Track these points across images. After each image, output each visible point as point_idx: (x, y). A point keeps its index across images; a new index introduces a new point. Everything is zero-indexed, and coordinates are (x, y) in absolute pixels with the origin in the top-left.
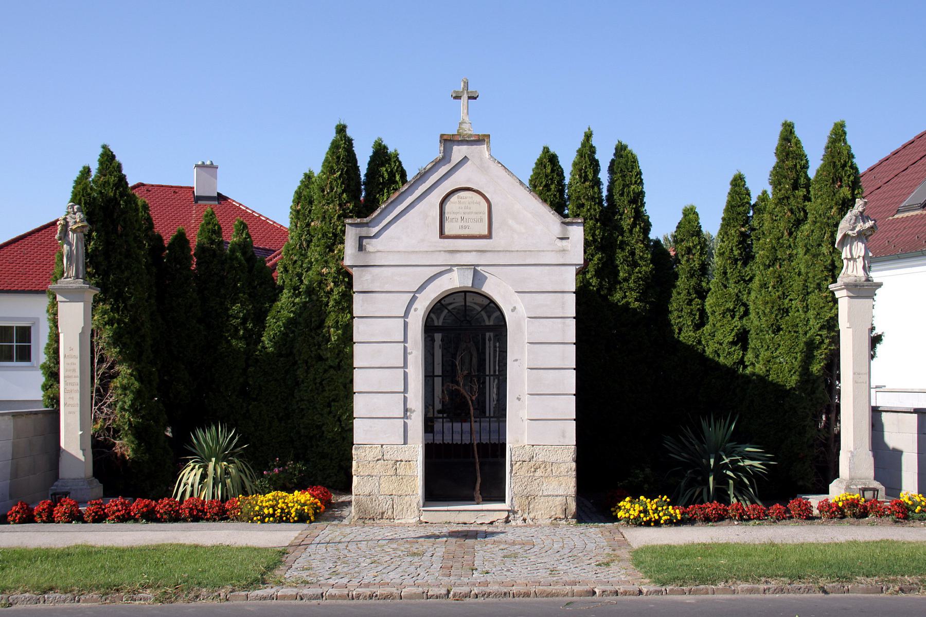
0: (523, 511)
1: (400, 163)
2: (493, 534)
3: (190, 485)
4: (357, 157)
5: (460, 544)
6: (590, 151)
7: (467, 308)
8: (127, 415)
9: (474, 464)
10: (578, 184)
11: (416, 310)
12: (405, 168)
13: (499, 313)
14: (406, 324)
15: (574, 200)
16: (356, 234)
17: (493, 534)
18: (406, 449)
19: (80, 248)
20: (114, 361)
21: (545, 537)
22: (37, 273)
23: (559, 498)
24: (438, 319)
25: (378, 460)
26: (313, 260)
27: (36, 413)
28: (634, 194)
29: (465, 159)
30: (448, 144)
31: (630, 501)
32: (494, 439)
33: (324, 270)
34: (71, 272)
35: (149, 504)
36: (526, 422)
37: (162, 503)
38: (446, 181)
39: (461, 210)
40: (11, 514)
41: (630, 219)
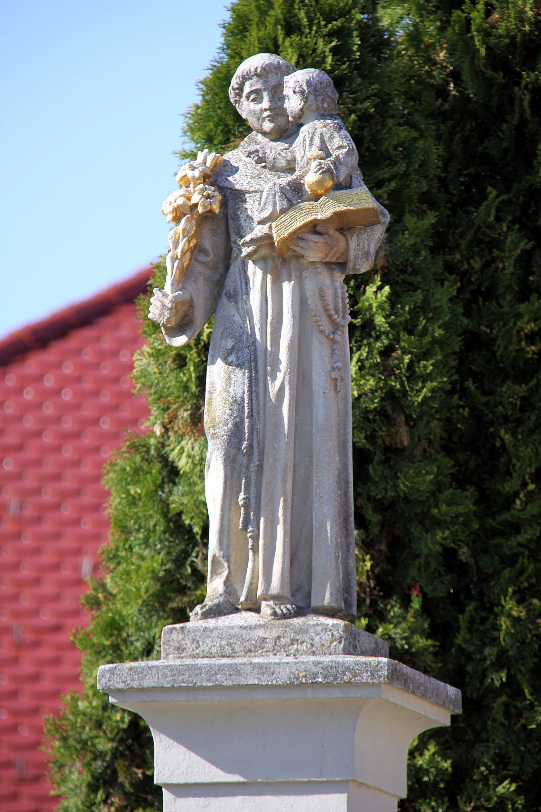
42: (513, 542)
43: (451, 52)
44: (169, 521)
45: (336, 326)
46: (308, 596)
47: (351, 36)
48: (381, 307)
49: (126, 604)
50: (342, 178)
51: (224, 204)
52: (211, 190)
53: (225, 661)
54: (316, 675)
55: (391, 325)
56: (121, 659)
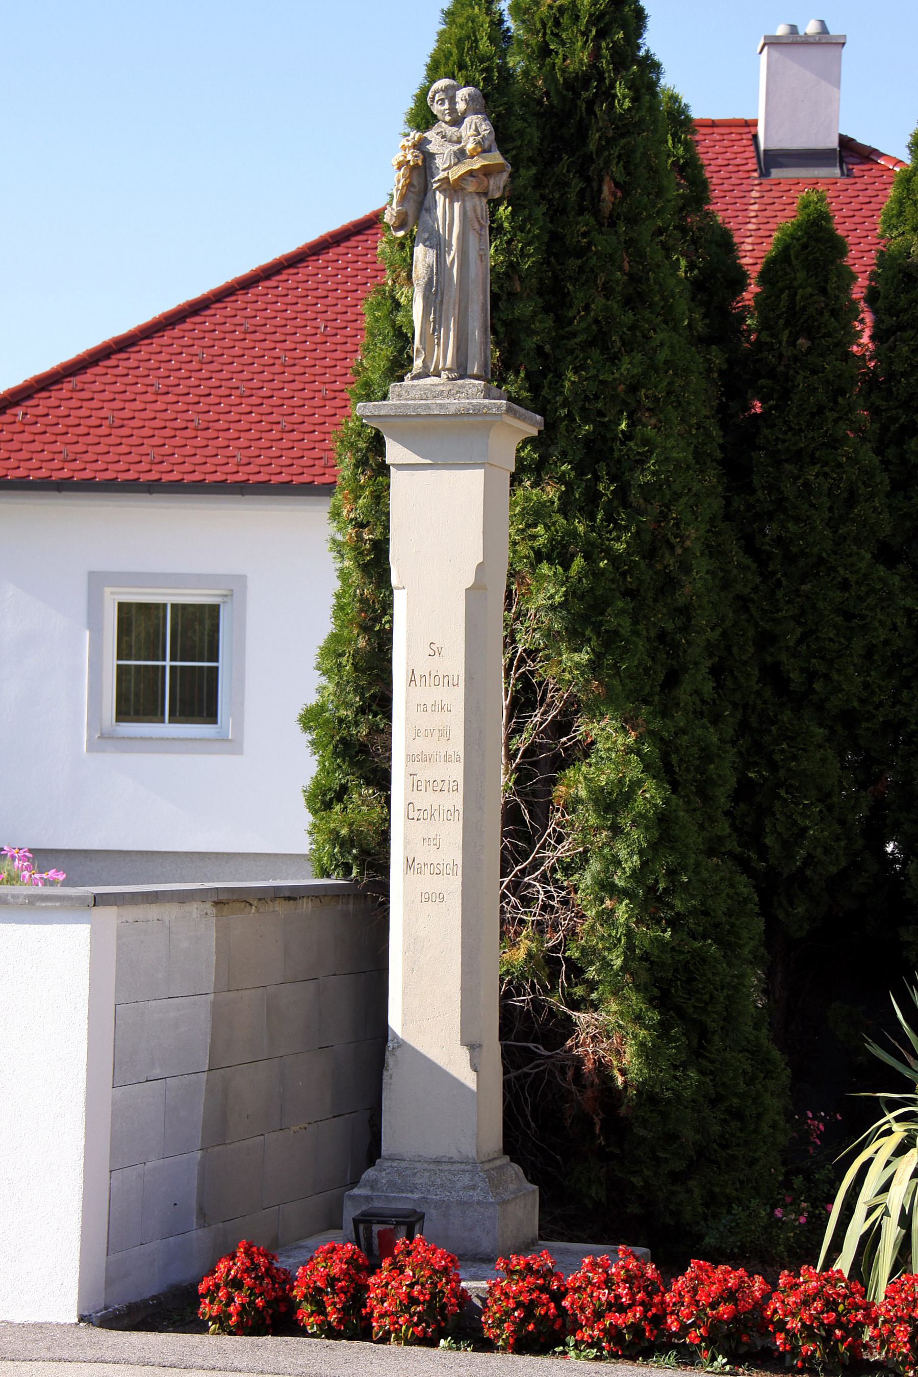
3: (895, 1213)
8: (622, 911)
19: (473, 255)
20: (572, 700)
22: (243, 425)
27: (292, 895)
34: (438, 352)
35: (740, 1287)
37: (794, 1286)
40: (212, 1293)
42: (572, 342)
43: (545, 81)
44: (395, 330)
45: (482, 227)
46: (466, 369)
47: (493, 71)
48: (507, 218)
49: (373, 373)
50: (486, 147)
51: (424, 160)
52: (417, 153)
53: (422, 402)
54: (469, 409)
55: (512, 227)
56: (370, 401)
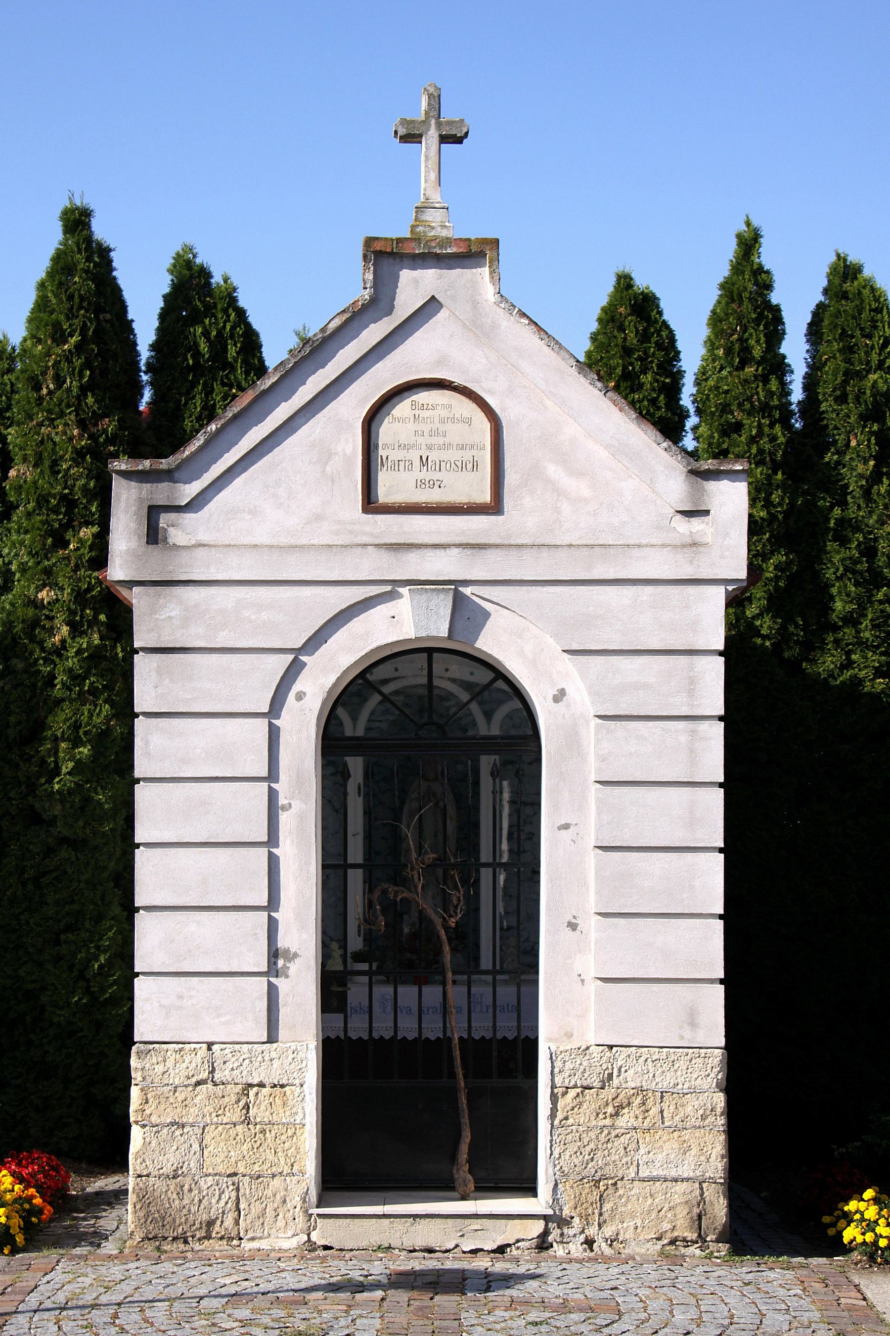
0: (586, 1219)
1: (241, 314)
2: (507, 1280)
4: (127, 295)
5: (421, 1309)
6: (756, 283)
7: (436, 692)
9: (455, 1091)
10: (724, 373)
11: (300, 696)
12: (256, 326)
13: (517, 704)
14: (274, 735)
15: (712, 413)
16: (141, 500)
17: (507, 1280)
18: (274, 1055)
21: (648, 1292)
23: (681, 1187)
24: (354, 719)
25: (198, 1083)
26: (14, 568)
28: (873, 395)
29: (431, 306)
30: (386, 263)
31: (876, 1200)
32: (507, 1029)
33: (44, 593)
36: (593, 986)
38: (380, 365)
39: (420, 440)
41: (866, 461)
